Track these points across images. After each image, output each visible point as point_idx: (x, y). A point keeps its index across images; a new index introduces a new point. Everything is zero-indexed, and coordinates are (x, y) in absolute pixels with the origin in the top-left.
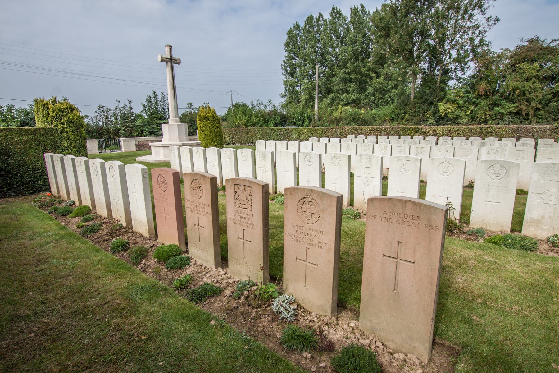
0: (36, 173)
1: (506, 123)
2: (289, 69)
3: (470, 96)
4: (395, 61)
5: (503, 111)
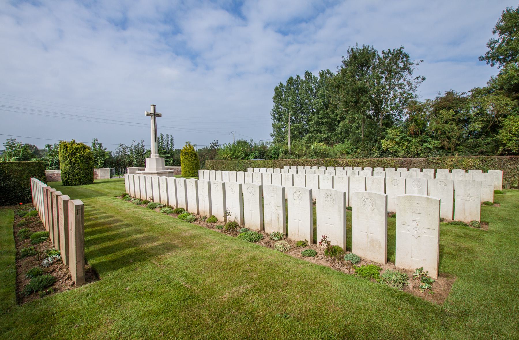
0: (26, 191)
1: (433, 155)
2: (276, 115)
3: (404, 134)
4: (344, 110)
5: (429, 146)
